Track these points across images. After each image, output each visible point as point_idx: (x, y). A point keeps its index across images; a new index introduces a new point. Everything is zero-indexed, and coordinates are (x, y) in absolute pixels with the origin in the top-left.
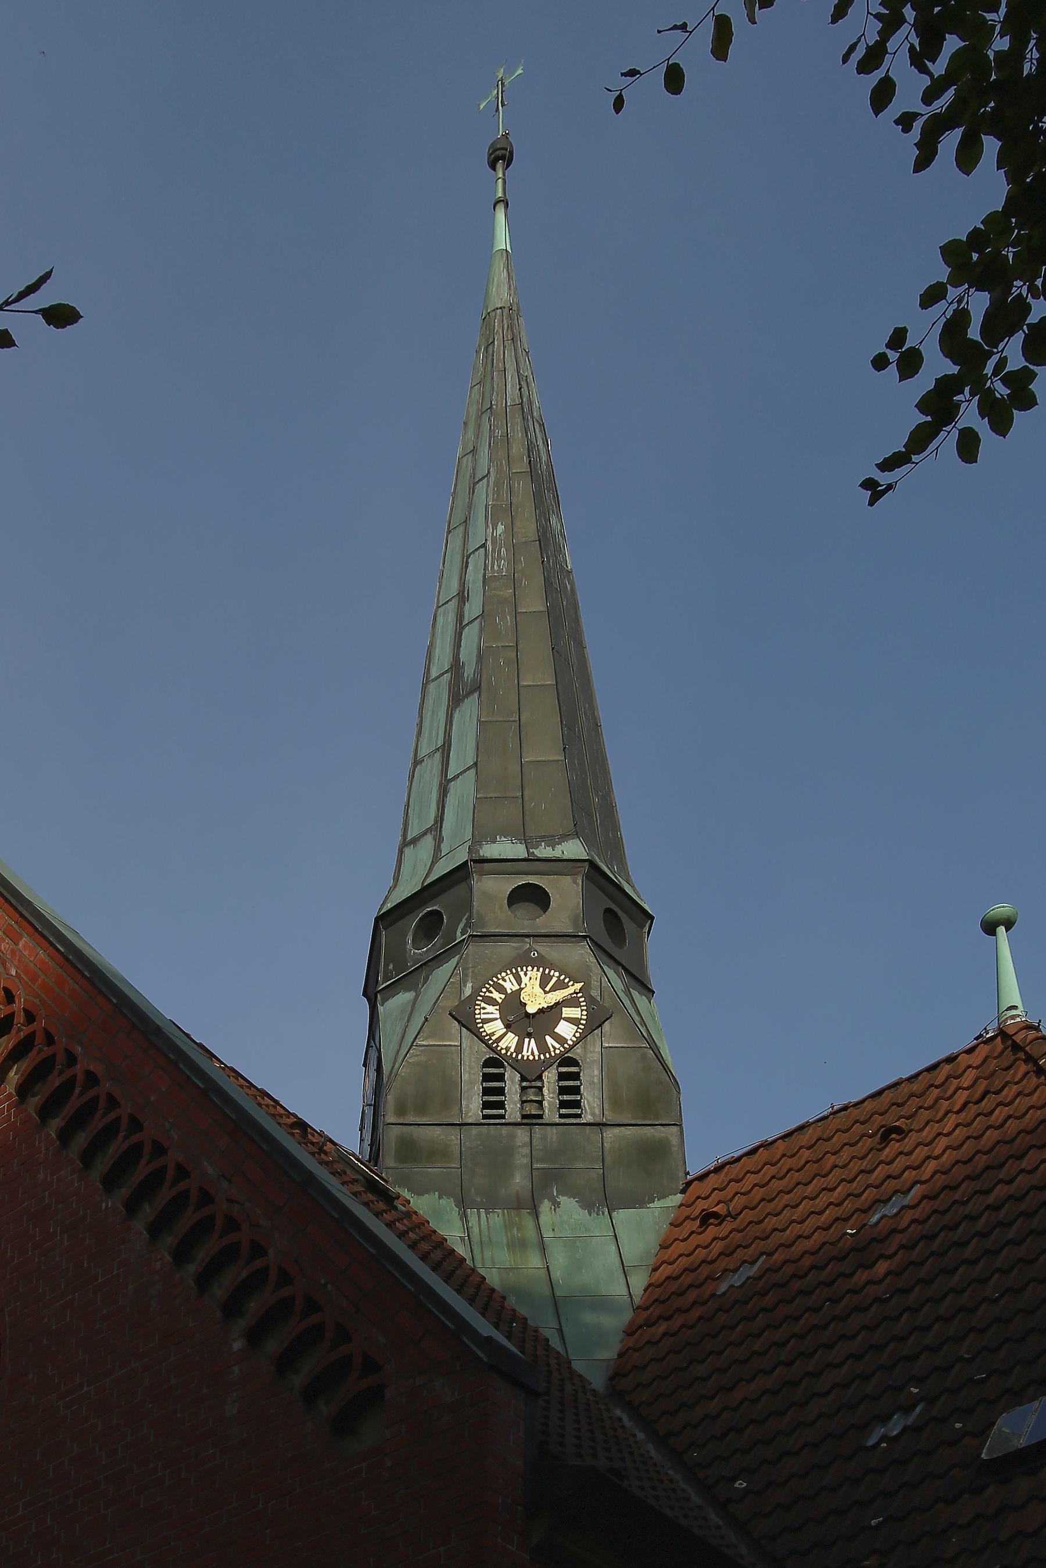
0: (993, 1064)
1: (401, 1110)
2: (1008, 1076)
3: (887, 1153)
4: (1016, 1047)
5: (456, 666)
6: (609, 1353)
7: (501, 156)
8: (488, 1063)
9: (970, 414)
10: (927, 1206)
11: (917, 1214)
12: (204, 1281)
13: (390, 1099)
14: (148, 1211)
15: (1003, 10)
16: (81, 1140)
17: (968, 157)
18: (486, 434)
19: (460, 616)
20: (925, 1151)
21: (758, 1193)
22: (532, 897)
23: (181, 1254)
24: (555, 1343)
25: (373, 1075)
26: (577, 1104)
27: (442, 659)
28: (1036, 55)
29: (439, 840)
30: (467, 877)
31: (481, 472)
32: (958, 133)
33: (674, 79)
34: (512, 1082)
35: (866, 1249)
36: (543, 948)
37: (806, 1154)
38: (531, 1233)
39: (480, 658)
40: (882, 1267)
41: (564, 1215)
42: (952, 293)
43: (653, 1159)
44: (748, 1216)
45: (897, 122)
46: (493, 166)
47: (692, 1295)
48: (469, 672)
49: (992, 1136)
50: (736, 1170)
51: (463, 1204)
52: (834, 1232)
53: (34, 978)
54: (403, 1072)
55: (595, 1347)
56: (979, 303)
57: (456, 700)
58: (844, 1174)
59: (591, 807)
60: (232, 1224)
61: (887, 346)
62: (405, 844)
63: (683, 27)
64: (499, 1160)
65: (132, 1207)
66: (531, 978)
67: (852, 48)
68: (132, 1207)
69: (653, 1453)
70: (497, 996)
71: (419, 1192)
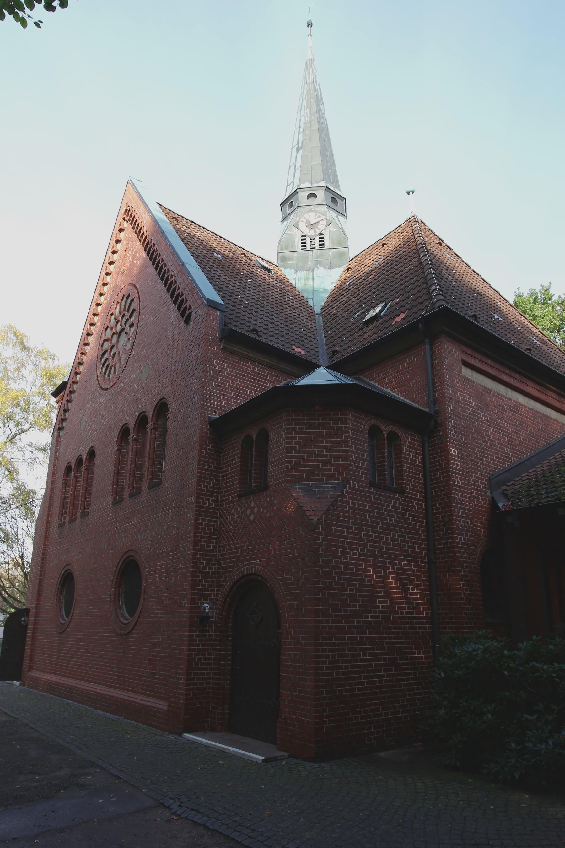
5: (298, 143)
7: (310, 25)
8: (303, 236)
27: (295, 143)
31: (304, 97)
34: (308, 240)
38: (311, 276)
39: (302, 141)
41: (320, 271)
43: (342, 255)
48: (300, 145)
55: (317, 304)
57: (298, 151)
62: (287, 186)
66: (312, 214)
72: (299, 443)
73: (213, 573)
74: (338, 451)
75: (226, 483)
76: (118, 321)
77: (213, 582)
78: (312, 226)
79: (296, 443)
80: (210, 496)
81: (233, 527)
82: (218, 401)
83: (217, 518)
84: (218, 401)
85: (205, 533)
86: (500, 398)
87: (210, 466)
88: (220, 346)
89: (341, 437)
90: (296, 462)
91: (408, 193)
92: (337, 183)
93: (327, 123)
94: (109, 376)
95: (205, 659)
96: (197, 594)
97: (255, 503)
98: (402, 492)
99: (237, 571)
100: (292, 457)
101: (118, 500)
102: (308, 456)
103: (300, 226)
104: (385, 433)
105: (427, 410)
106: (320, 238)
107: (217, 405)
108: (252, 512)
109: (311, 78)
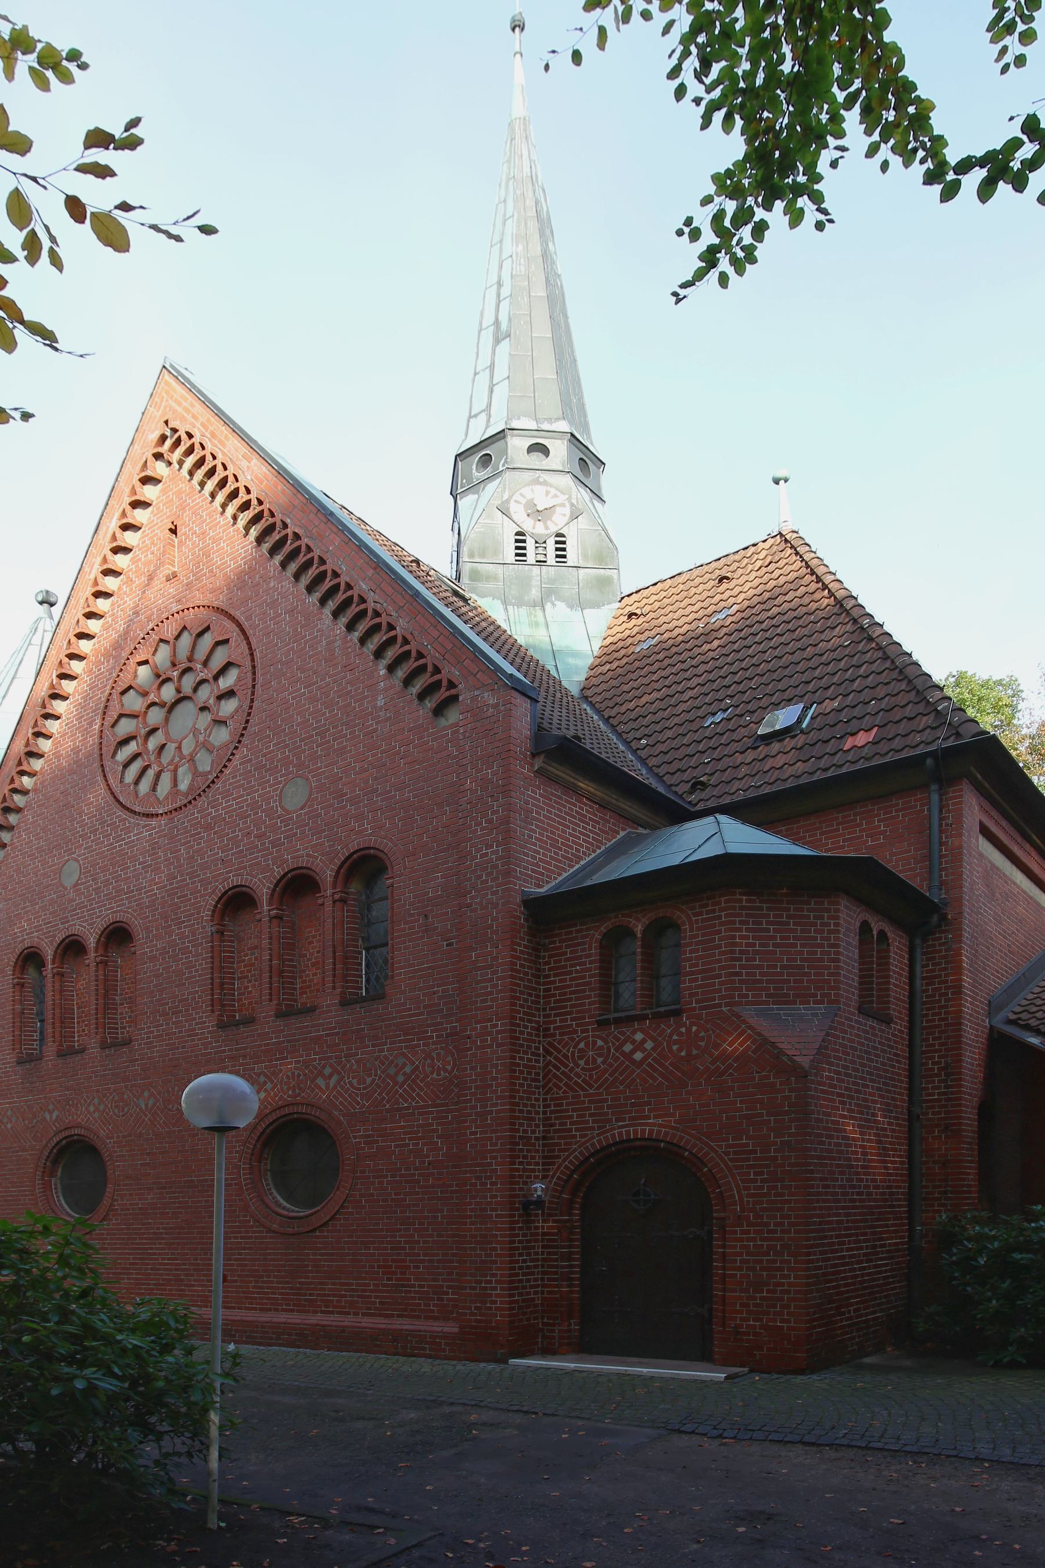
0: (775, 548)
1: (471, 555)
2: (782, 555)
3: (720, 590)
4: (786, 541)
5: (497, 323)
6: (582, 677)
8: (517, 534)
9: (724, 264)
10: (739, 615)
11: (733, 619)
12: (363, 641)
13: (465, 550)
14: (331, 605)
15: (747, 48)
16: (293, 567)
17: (728, 123)
18: (512, 193)
19: (499, 295)
20: (739, 589)
21: (657, 605)
22: (540, 449)
23: (350, 627)
24: (553, 672)
25: (456, 536)
26: (564, 557)
27: (489, 319)
28: (763, 76)
29: (489, 416)
30: (504, 437)
32: (724, 111)
33: (577, 57)
34: (530, 544)
35: (708, 635)
36: (545, 476)
37: (681, 587)
39: (510, 319)
40: (716, 643)
42: (717, 200)
43: (604, 583)
44: (651, 615)
45: (693, 101)
46: (513, 30)
47: (623, 652)
48: (504, 326)
49: (773, 583)
50: (645, 593)
51: (505, 603)
52: (693, 626)
53: (261, 482)
54: (472, 536)
55: (573, 673)
56: (731, 207)
57: (497, 341)
58: (701, 598)
59: (572, 402)
60: (377, 614)
61: (684, 224)
62: (470, 417)
63: (581, 29)
64: (525, 583)
65: (323, 601)
66: (540, 490)
67: (673, 51)
68: (323, 601)
69: (602, 725)
70: (520, 499)
71: (483, 596)
73: (537, 1139)
74: (821, 960)
77: (537, 1151)
78: (538, 514)
79: (748, 945)
82: (533, 864)
83: (539, 1055)
84: (533, 864)
85: (525, 1079)
86: (1006, 882)
87: (526, 974)
88: (532, 765)
90: (747, 974)
91: (777, 482)
92: (585, 427)
93: (562, 286)
94: (154, 788)
95: (532, 1261)
96: (517, 1170)
100: (741, 967)
102: (769, 967)
103: (512, 510)
106: (557, 542)
107: (533, 871)
109: (526, 170)
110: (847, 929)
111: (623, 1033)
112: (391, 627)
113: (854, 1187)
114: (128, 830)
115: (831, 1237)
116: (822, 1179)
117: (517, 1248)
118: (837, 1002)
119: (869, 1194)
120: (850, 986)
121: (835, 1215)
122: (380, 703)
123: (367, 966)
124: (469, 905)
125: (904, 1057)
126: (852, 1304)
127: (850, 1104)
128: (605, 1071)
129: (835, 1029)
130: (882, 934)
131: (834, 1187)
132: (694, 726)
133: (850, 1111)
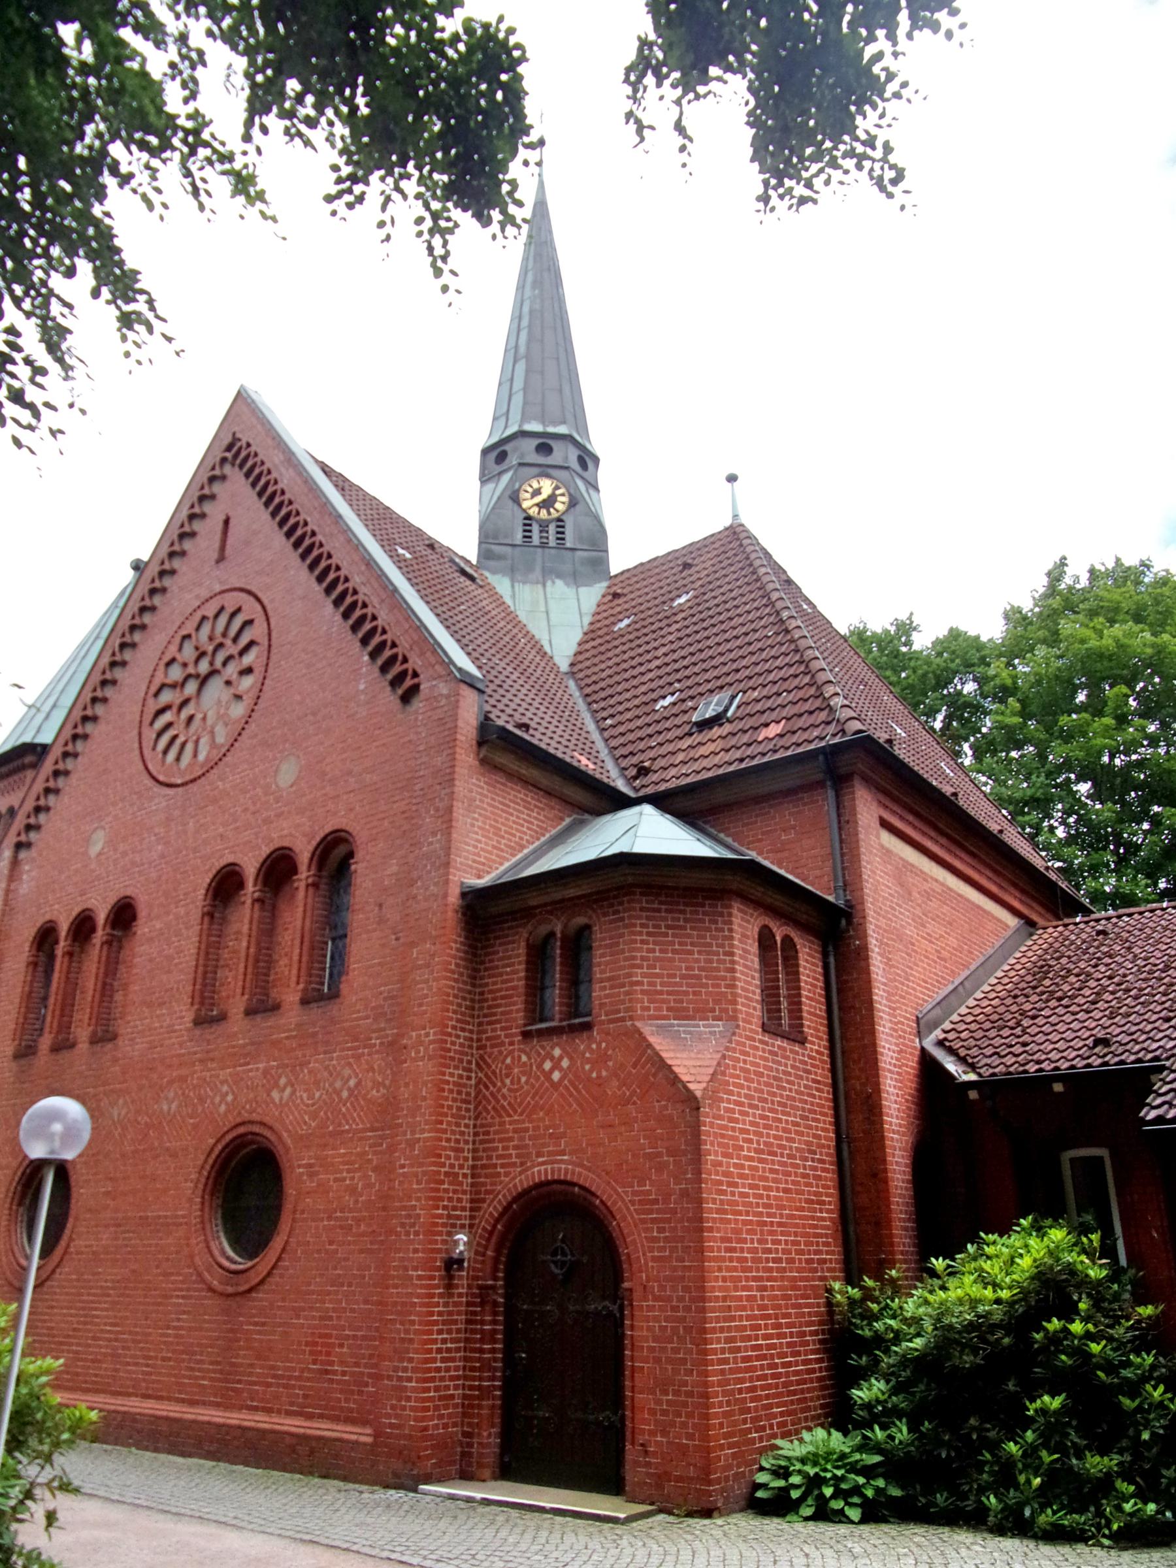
72: (654, 951)
73: (465, 1176)
75: (489, 1007)
76: (203, 654)
79: (649, 951)
80: (463, 1030)
81: (510, 1090)
89: (723, 946)
94: (178, 759)
97: (563, 1049)
98: (802, 1042)
99: (521, 1173)
101: (208, 1016)
104: (778, 939)
105: (831, 898)
108: (556, 1066)
110: (744, 936)
111: (543, 1047)
112: (374, 618)
113: (769, 1251)
114: (151, 798)
115: (741, 1318)
116: (723, 1240)
117: (436, 1323)
118: (735, 1018)
119: (791, 1261)
120: (751, 1000)
121: (744, 1288)
122: (362, 687)
123: (332, 958)
124: (414, 897)
125: (825, 1085)
126: (774, 1416)
127: (758, 1143)
128: (528, 1092)
129: (734, 1050)
130: (787, 939)
131: (742, 1250)
132: (647, 709)
133: (757, 1151)
